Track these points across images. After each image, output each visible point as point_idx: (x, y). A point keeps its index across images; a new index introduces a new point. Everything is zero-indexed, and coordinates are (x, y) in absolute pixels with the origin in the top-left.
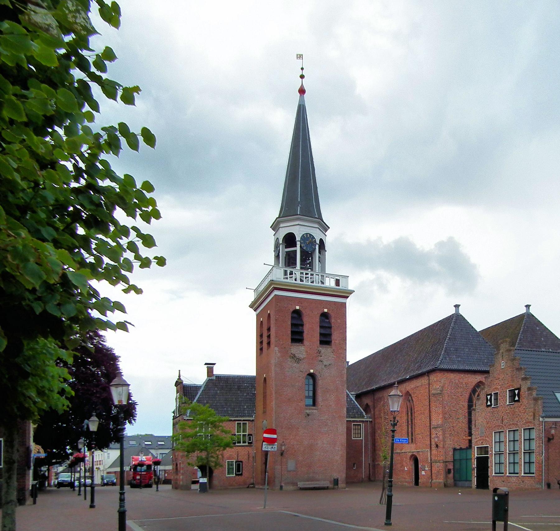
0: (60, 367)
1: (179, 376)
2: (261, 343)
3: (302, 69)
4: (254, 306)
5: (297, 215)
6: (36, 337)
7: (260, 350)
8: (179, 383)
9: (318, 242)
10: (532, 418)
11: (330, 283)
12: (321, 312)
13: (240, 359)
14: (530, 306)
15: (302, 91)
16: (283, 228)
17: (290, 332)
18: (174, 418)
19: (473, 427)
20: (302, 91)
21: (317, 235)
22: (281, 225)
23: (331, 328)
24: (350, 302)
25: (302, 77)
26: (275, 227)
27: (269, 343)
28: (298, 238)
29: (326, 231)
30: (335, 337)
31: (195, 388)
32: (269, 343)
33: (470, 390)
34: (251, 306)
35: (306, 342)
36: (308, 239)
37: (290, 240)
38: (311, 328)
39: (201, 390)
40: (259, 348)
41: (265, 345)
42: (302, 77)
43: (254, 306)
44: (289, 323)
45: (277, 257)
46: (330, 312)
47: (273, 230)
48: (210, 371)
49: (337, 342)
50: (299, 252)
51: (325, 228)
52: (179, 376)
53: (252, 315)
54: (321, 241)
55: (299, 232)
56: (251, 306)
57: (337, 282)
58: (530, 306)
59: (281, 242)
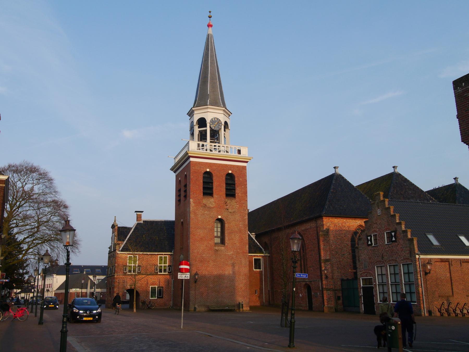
1: (115, 221)
4: (174, 169)
9: (223, 123)
12: (226, 173)
14: (396, 167)
17: (202, 188)
19: (357, 262)
23: (233, 183)
28: (208, 121)
30: (238, 191)
34: (172, 169)
35: (215, 195)
38: (219, 186)
43: (174, 169)
44: (202, 181)
45: (192, 134)
46: (234, 173)
47: (189, 116)
48: (139, 217)
49: (240, 194)
53: (173, 176)
54: (226, 123)
56: (172, 169)
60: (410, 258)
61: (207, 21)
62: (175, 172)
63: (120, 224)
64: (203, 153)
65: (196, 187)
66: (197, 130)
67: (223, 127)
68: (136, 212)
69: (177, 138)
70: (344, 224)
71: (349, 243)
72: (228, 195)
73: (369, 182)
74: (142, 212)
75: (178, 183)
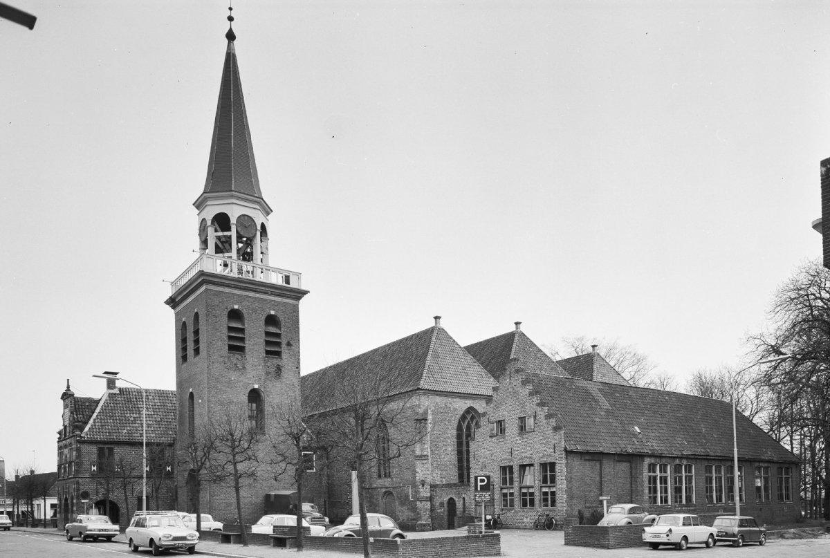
0: (548, 424)
1: (68, 387)
2: (185, 349)
3: (230, 9)
5: (232, 191)
6: (254, 402)
7: (183, 357)
8: (67, 396)
9: (259, 227)
10: (552, 450)
11: (277, 279)
13: (153, 367)
14: (520, 323)
15: (231, 36)
16: (211, 207)
18: (60, 440)
19: (471, 458)
20: (231, 36)
21: (259, 218)
22: (209, 203)
23: (280, 337)
24: (303, 304)
25: (231, 19)
26: (200, 204)
27: (197, 351)
28: (233, 220)
29: (268, 214)
31: (94, 403)
32: (197, 351)
33: (458, 417)
34: (167, 302)
36: (245, 221)
37: (222, 221)
39: (101, 404)
40: (181, 354)
41: (190, 351)
42: (231, 19)
45: (205, 243)
47: (198, 208)
48: (111, 384)
50: (233, 234)
51: (267, 211)
52: (68, 387)
54: (263, 225)
55: (234, 212)
57: (287, 279)
58: (520, 323)
59: (209, 223)
60: (553, 453)
61: (228, 13)
62: (173, 307)
63: (79, 392)
64: (276, 361)
65: (215, 336)
66: (212, 235)
67: (258, 234)
68: (106, 373)
69: (181, 252)
70: (449, 405)
71: (455, 432)
72: (31, 26)
73: (351, 363)
74: (116, 373)
75: (182, 328)
